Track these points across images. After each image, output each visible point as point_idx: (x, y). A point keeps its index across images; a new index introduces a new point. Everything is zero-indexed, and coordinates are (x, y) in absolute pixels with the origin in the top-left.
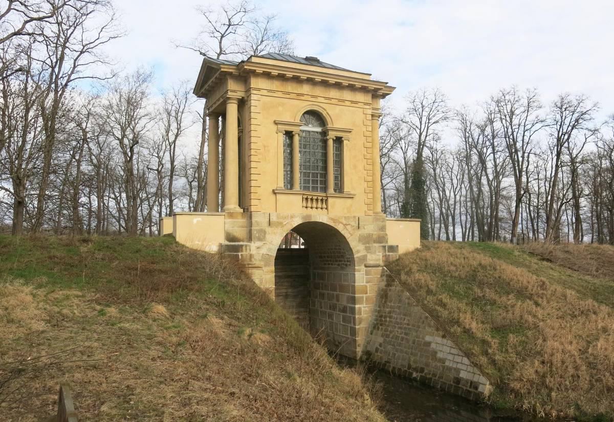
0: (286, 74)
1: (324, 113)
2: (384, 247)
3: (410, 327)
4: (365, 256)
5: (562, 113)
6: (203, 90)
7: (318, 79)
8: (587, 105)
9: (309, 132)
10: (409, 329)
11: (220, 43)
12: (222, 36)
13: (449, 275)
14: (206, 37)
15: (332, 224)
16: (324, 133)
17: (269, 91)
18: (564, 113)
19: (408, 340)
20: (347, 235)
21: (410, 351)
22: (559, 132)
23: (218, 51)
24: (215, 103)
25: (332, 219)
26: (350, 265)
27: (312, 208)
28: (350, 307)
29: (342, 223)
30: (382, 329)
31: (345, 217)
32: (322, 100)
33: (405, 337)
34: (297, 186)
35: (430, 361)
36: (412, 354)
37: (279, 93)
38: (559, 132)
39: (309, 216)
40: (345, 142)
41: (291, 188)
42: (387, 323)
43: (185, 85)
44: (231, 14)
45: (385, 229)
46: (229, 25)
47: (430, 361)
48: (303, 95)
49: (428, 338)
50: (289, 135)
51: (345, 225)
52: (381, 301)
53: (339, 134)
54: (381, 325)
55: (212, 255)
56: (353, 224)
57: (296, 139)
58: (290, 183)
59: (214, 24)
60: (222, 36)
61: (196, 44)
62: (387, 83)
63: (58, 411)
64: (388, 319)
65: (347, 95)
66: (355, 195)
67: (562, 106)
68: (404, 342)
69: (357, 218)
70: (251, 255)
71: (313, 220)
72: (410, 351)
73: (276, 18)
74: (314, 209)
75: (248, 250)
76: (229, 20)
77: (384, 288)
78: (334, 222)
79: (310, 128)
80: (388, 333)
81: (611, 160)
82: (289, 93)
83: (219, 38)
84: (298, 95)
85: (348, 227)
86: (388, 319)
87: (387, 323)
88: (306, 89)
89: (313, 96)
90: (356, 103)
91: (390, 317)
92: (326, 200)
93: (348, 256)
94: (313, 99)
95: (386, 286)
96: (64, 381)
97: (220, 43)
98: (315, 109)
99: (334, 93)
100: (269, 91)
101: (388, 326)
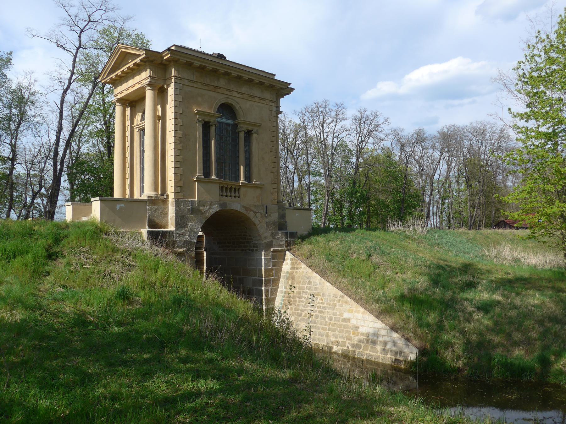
0: (206, 66)
1: (237, 107)
2: (286, 233)
3: (325, 305)
5: (360, 124)
6: (113, 76)
8: (381, 120)
9: (223, 123)
10: (324, 308)
11: (80, 37)
12: (82, 31)
14: (66, 29)
15: (244, 211)
16: (236, 125)
17: (190, 81)
18: (363, 125)
19: (324, 318)
20: (257, 222)
21: (327, 327)
22: (358, 140)
23: (77, 45)
24: (128, 89)
25: (244, 207)
26: (256, 250)
27: (235, 197)
28: (256, 289)
29: (252, 211)
30: (291, 309)
31: (255, 206)
32: (235, 94)
33: (320, 315)
35: (351, 335)
36: (329, 330)
37: (199, 84)
38: (358, 140)
40: (255, 135)
42: (297, 303)
43: (29, 77)
44: (90, 11)
45: (285, 217)
46: (90, 21)
47: (351, 335)
48: (219, 88)
49: (346, 315)
50: (206, 126)
51: (255, 213)
52: (288, 283)
53: (250, 128)
54: (290, 304)
55: (393, 219)
56: (261, 211)
57: (213, 130)
59: (73, 18)
60: (82, 31)
61: (54, 37)
62: (290, 84)
64: (297, 299)
65: (257, 92)
66: (263, 185)
67: (361, 119)
68: (319, 319)
69: (265, 206)
71: (228, 208)
72: (327, 327)
73: (132, 20)
74: (233, 198)
76: (89, 16)
77: (289, 270)
78: (246, 210)
79: (224, 120)
80: (299, 312)
83: (79, 32)
84: (216, 87)
85: (258, 215)
86: (297, 299)
87: (297, 303)
88: (222, 83)
90: (264, 99)
91: (299, 298)
92: (239, 189)
93: (255, 242)
94: (228, 93)
95: (291, 269)
97: (80, 37)
98: (230, 102)
99: (245, 89)
100: (190, 81)
101: (298, 305)
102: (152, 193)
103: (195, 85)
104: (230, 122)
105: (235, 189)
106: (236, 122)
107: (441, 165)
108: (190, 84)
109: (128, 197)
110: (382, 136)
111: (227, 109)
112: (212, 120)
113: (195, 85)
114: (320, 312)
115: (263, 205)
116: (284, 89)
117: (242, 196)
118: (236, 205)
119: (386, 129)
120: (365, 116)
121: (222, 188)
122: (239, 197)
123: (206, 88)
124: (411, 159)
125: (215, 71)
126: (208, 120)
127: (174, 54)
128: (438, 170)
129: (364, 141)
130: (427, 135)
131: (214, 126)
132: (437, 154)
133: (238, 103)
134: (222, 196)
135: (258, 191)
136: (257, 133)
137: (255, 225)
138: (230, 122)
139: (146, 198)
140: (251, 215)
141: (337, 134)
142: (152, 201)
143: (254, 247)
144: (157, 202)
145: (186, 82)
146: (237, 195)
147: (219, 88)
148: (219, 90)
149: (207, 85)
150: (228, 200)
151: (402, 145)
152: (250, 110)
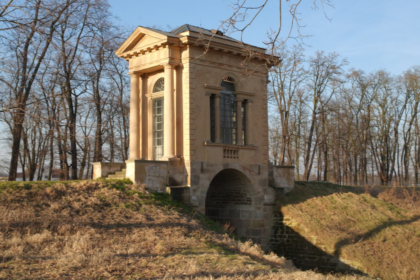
4: (263, 196)
7: (226, 50)
13: (370, 256)
15: (241, 170)
25: (242, 166)
32: (235, 69)
34: (218, 140)
37: (207, 62)
39: (227, 164)
41: (214, 142)
48: (223, 64)
50: (213, 97)
53: (246, 97)
57: (217, 101)
58: (213, 139)
63: (76, 166)
66: (257, 147)
70: (189, 196)
71: (230, 168)
75: (188, 193)
81: (68, 3)
82: (214, 63)
88: (225, 60)
89: (230, 66)
92: (237, 151)
94: (229, 68)
96: (78, 186)
102: (171, 156)
103: (205, 64)
104: (229, 92)
105: (234, 151)
106: (235, 93)
107: (407, 110)
108: (201, 63)
109: (149, 159)
110: (342, 78)
111: (230, 84)
112: (217, 92)
113: (205, 64)
114: (310, 258)
115: (256, 165)
116: (275, 61)
117: (240, 157)
118: (235, 165)
119: (346, 70)
120: (323, 57)
121: (225, 150)
122: (237, 158)
123: (213, 65)
124: (374, 103)
125: (220, 51)
126: (214, 93)
127: (191, 40)
128: (404, 114)
129: (322, 84)
130: (391, 76)
131: (219, 98)
132: (402, 97)
133: (237, 77)
134: (224, 157)
135: (253, 152)
136: (252, 102)
137: (250, 181)
138: (229, 92)
139: (167, 160)
140: (247, 173)
141: (294, 78)
142: (171, 162)
143: (248, 200)
144: (176, 162)
145: (198, 62)
146: (236, 156)
147: (223, 64)
148: (222, 67)
149: (214, 63)
150: (229, 161)
151: (364, 87)
152: (247, 84)
